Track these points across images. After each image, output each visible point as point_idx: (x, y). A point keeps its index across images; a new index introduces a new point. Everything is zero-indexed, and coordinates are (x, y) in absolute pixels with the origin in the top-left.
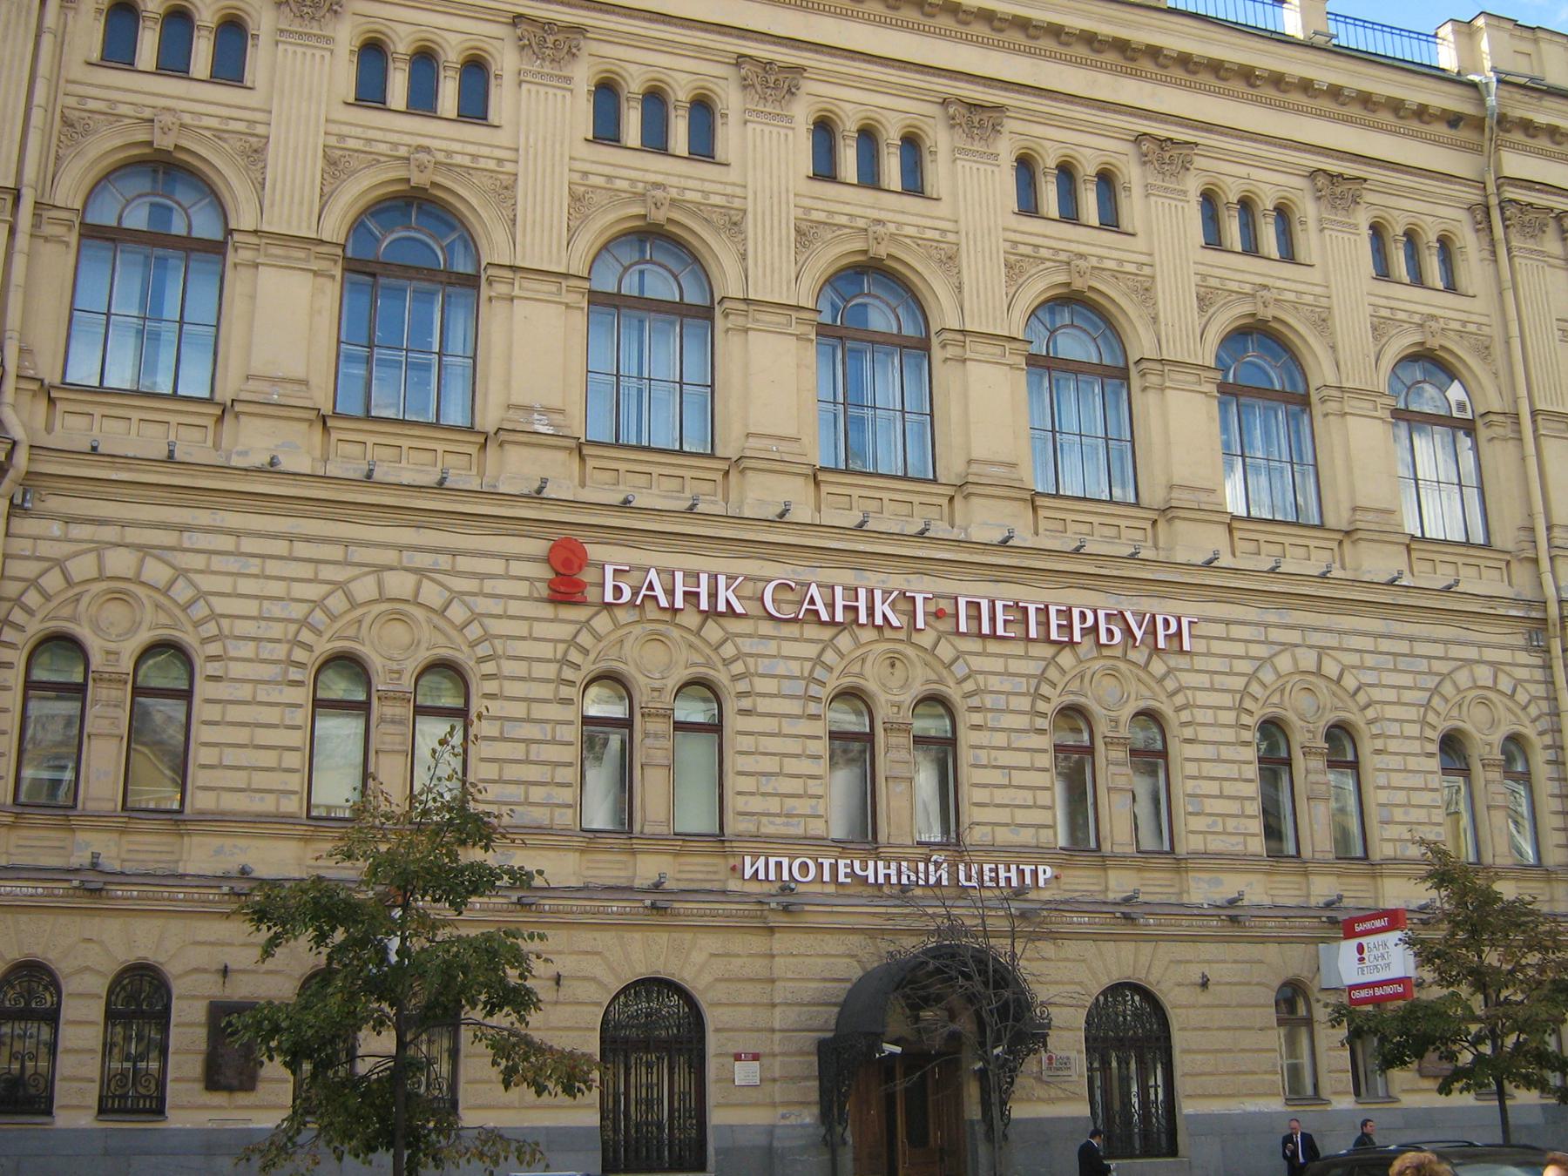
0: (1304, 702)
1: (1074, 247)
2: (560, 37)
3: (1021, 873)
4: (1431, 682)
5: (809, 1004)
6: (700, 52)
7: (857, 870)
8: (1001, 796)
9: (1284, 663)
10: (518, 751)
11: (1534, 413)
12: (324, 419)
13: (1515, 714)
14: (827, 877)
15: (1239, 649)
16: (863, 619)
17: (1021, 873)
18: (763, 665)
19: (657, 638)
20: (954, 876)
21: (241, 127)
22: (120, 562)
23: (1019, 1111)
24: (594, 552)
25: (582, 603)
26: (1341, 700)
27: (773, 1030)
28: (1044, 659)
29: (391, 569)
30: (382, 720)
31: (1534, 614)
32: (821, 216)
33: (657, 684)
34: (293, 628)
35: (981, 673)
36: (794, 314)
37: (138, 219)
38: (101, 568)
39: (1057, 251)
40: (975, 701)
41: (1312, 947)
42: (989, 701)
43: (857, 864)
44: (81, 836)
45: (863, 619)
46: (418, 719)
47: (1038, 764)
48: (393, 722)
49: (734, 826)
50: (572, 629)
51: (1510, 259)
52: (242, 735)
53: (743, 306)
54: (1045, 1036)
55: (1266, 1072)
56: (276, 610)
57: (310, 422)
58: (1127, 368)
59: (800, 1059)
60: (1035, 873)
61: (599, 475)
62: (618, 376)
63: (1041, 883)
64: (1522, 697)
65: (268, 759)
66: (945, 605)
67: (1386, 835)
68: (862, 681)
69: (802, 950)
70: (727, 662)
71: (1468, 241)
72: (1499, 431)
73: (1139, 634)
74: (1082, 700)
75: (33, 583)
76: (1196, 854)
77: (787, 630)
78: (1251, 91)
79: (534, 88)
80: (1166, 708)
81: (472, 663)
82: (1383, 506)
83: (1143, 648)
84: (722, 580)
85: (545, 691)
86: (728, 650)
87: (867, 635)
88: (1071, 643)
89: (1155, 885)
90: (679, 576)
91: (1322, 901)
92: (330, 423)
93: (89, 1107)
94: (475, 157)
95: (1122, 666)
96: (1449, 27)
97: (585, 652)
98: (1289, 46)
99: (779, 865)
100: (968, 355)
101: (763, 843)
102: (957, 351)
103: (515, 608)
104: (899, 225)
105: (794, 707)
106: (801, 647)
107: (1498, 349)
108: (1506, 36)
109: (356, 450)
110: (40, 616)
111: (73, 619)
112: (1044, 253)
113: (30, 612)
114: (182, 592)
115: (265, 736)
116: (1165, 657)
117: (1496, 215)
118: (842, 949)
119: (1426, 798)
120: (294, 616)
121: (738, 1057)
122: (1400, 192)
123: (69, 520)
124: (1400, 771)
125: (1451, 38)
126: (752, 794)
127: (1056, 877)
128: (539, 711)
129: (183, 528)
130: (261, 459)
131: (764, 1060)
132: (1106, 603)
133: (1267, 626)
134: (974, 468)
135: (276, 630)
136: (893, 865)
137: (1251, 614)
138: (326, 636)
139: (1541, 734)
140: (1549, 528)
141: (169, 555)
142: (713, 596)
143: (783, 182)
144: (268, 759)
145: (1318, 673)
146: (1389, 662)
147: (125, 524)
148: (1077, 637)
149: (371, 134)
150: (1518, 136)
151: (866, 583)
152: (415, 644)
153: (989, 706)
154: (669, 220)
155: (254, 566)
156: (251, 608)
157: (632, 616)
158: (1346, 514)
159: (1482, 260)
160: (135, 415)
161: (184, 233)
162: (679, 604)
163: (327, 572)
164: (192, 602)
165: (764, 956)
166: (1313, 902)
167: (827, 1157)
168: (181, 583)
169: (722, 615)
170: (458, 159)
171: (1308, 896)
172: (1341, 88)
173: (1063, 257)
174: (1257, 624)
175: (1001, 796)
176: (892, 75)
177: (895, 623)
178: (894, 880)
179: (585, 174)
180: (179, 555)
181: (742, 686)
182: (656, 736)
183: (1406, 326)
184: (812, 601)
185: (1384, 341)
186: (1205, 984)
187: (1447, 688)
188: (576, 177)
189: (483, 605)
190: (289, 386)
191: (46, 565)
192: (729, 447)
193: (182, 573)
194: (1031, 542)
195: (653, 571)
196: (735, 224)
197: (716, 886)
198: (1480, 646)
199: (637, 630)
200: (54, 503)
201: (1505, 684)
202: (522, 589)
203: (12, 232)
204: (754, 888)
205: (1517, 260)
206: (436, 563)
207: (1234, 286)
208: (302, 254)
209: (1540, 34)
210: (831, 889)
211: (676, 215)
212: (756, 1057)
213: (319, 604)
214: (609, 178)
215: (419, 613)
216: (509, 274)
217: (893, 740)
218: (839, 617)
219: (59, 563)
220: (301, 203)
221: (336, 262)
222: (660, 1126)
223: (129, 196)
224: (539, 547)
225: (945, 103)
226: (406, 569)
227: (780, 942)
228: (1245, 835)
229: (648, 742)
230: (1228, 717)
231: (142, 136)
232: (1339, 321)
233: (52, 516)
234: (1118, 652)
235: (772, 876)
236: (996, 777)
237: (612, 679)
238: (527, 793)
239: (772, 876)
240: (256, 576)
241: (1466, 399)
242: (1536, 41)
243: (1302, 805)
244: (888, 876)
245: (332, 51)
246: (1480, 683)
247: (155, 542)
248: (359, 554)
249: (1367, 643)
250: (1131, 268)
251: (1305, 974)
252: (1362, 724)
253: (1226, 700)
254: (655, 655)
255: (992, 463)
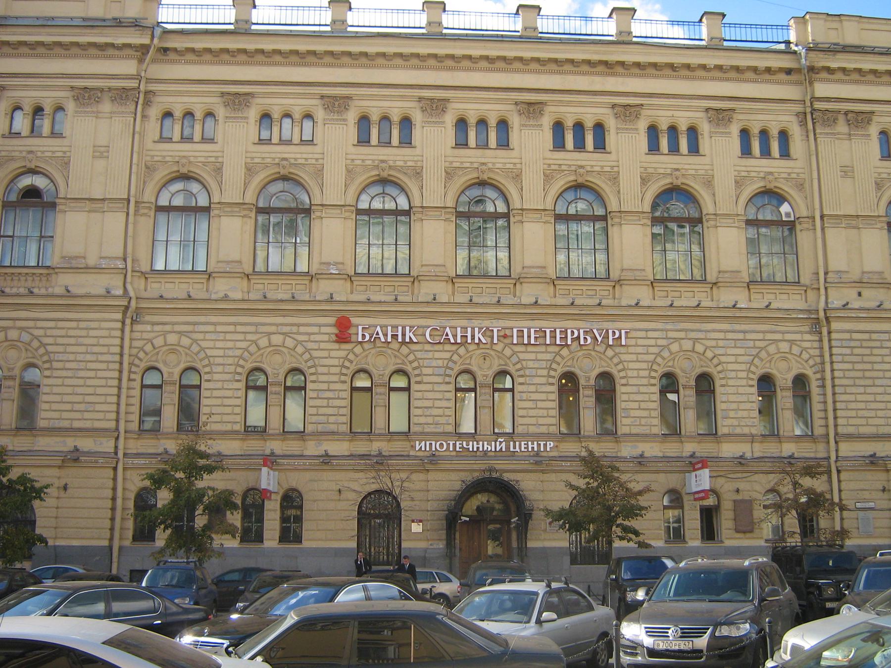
0: (686, 364)
1: (579, 163)
2: (341, 101)
3: (539, 445)
4: (754, 351)
5: (442, 500)
6: (402, 98)
7: (465, 446)
8: (532, 413)
9: (675, 347)
10: (325, 402)
11: (822, 217)
12: (350, 277)
13: (802, 364)
14: (451, 449)
15: (652, 342)
16: (469, 341)
17: (539, 445)
18: (426, 363)
19: (381, 354)
20: (508, 447)
21: (213, 159)
22: (172, 339)
23: (530, 544)
24: (354, 320)
25: (349, 342)
26: (705, 362)
27: (428, 511)
28: (348, 350)
29: (683, 339)
30: (377, 394)
31: (813, 316)
32: (458, 165)
33: (381, 373)
34: (236, 359)
35: (524, 360)
36: (443, 211)
37: (178, 201)
38: (165, 342)
39: (570, 166)
40: (521, 373)
41: (682, 475)
42: (528, 372)
43: (464, 443)
44: (162, 441)
45: (469, 341)
46: (391, 392)
47: (550, 398)
48: (275, 394)
49: (414, 429)
50: (346, 353)
51: (815, 139)
52: (219, 402)
53: (420, 210)
54: (531, 514)
55: (656, 529)
56: (230, 353)
57: (346, 279)
58: (702, 218)
59: (439, 522)
60: (545, 445)
61: (561, 292)
62: (396, 245)
63: (548, 449)
64: (805, 356)
65: (228, 410)
66: (508, 332)
67: (725, 424)
68: (470, 367)
69: (440, 479)
70: (411, 362)
71: (796, 132)
72: (806, 226)
73: (600, 339)
74: (572, 369)
75: (142, 349)
76: (724, 435)
77: (437, 347)
78: (675, 73)
79: (330, 126)
80: (614, 371)
81: (306, 369)
82: (734, 269)
83: (603, 345)
84: (408, 329)
85: (335, 378)
86: (411, 357)
87: (472, 347)
88: (567, 345)
89: (703, 449)
90: (459, 329)
91: (689, 454)
92: (353, 279)
93: (276, 540)
94: (306, 159)
95: (593, 353)
96: (792, 21)
97: (351, 362)
98: (71, 28)
99: (431, 444)
100: (525, 219)
101: (424, 435)
102: (520, 218)
103: (323, 345)
104: (494, 164)
105: (439, 379)
106: (442, 355)
107: (807, 185)
108: (822, 22)
109: (261, 286)
110: (144, 361)
111: (156, 361)
112: (563, 167)
113: (141, 360)
114: (195, 348)
115: (227, 402)
116: (614, 348)
117: (809, 117)
118: (457, 478)
119: (748, 406)
120: (237, 355)
121: (413, 521)
122: (660, 107)
123: (153, 324)
124: (734, 394)
125: (794, 26)
126: (421, 416)
127: (557, 446)
128: (333, 386)
129: (195, 324)
130: (221, 295)
131: (424, 522)
132: (583, 325)
133: (667, 330)
134: (526, 270)
135: (230, 361)
136: (481, 443)
137: (660, 326)
138: (249, 362)
139: (814, 373)
140: (826, 273)
141: (190, 335)
142: (404, 335)
143: (439, 151)
144: (228, 410)
145: (693, 351)
146: (732, 343)
147: (174, 324)
148: (569, 342)
149: (264, 155)
150: (824, 75)
151: (611, 327)
152: (789, 369)
153: (528, 374)
154: (389, 175)
155: (221, 337)
156: (221, 353)
157: (371, 345)
158: (715, 275)
159: (802, 140)
160: (177, 281)
161: (574, 213)
162: (389, 339)
163: (249, 337)
164: (199, 352)
165: (425, 481)
166: (684, 455)
167: (448, 561)
168: (194, 345)
169: (407, 343)
170: (300, 161)
171: (781, 452)
172: (722, 66)
173: (573, 168)
174: (662, 330)
175: (532, 413)
176: (491, 95)
177: (484, 341)
178: (481, 449)
179: (353, 160)
180: (193, 334)
181: (417, 372)
182: (380, 394)
183: (755, 179)
184: (447, 335)
185: (742, 188)
186: (65, 488)
187: (763, 354)
188: (349, 162)
189: (310, 345)
190: (234, 264)
191: (145, 342)
192: (711, 277)
193: (195, 341)
194: (709, 304)
195: (378, 327)
196: (418, 173)
197: (405, 453)
198: (783, 333)
199: (373, 351)
200: (148, 318)
201: (699, 348)
202: (326, 338)
203: (128, 214)
204: (419, 454)
205: (819, 140)
206: (291, 330)
207: (662, 171)
208: (237, 209)
209: (843, 18)
210: (454, 453)
211: (392, 173)
212: (421, 521)
213: (246, 349)
214: (363, 160)
215: (695, 355)
216: (320, 208)
217: (483, 391)
218: (459, 341)
219: (150, 341)
220: (237, 189)
221: (150, 210)
222: (594, 547)
223: (759, 205)
224: (332, 320)
225: (516, 104)
226: (280, 333)
227: (431, 476)
228: (651, 425)
229: (377, 396)
230: (744, 375)
231: (175, 169)
232: (227, 172)
233: (148, 323)
234: (591, 347)
235: (428, 449)
236: (530, 404)
237: (401, 372)
238: (328, 419)
239: (428, 449)
240: (222, 340)
241: (791, 211)
242: (841, 21)
243: (780, 411)
244: (478, 448)
245: (445, 127)
246: (781, 351)
247: (185, 330)
248: (262, 329)
249: (721, 335)
250: (608, 169)
251: (678, 487)
252: (715, 373)
253: (644, 366)
254: (381, 360)
255: (533, 267)
